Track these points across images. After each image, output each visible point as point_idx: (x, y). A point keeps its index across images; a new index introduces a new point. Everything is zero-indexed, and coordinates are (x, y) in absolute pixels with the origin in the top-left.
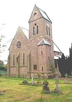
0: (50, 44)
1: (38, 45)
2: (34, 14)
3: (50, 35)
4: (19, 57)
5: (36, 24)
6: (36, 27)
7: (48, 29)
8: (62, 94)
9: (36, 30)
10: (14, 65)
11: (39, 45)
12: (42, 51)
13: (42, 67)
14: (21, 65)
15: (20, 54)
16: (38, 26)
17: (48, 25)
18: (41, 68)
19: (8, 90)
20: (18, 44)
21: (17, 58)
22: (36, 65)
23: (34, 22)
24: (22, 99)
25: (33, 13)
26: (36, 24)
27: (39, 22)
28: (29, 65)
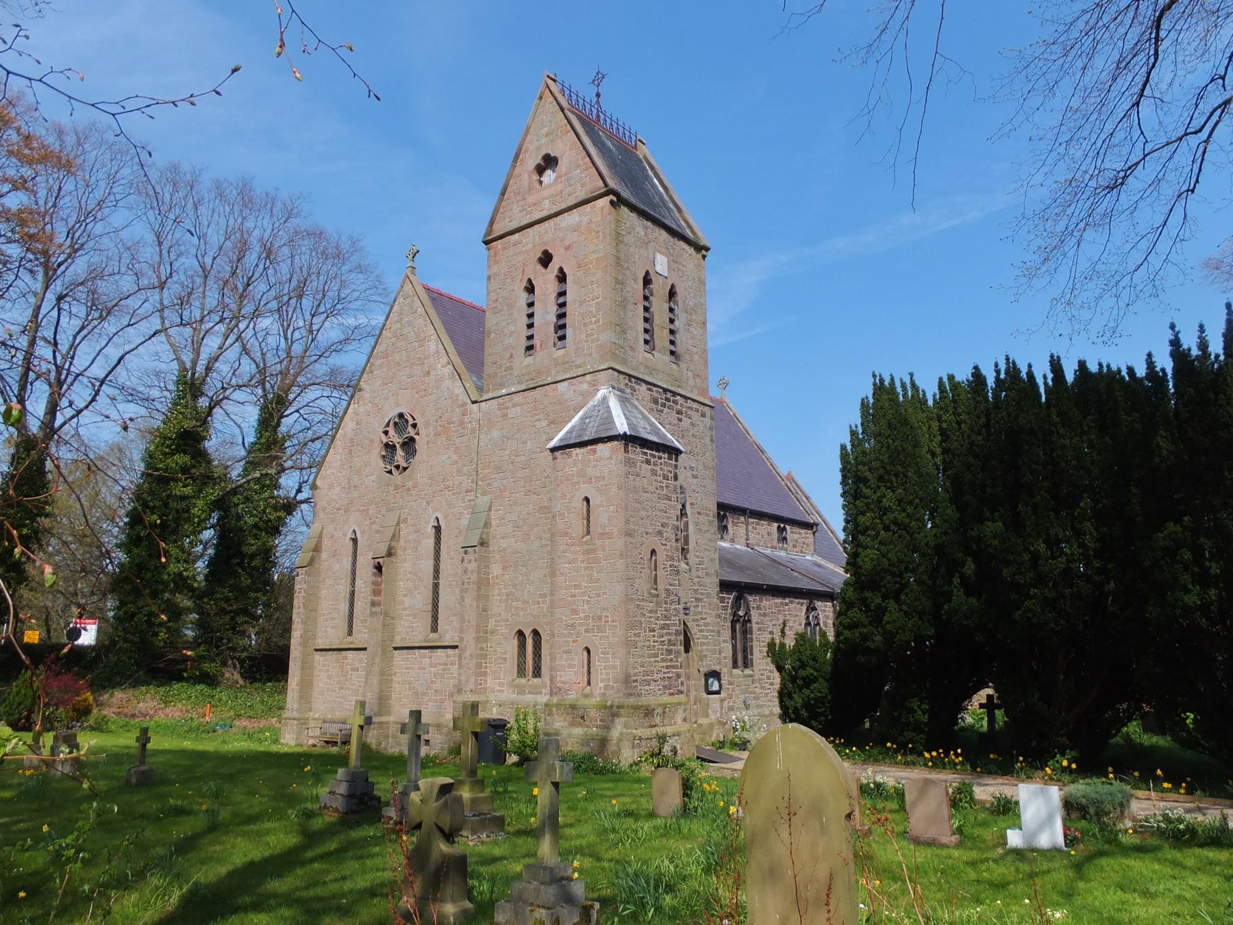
0: (711, 404)
1: (552, 444)
2: (540, 170)
4: (390, 554)
5: (546, 259)
6: (546, 282)
7: (659, 307)
9: (546, 315)
12: (587, 500)
14: (412, 627)
16: (562, 277)
17: (661, 265)
19: (119, 156)
22: (536, 633)
23: (532, 242)
24: (141, 618)
26: (546, 259)
27: (572, 238)
28: (470, 635)
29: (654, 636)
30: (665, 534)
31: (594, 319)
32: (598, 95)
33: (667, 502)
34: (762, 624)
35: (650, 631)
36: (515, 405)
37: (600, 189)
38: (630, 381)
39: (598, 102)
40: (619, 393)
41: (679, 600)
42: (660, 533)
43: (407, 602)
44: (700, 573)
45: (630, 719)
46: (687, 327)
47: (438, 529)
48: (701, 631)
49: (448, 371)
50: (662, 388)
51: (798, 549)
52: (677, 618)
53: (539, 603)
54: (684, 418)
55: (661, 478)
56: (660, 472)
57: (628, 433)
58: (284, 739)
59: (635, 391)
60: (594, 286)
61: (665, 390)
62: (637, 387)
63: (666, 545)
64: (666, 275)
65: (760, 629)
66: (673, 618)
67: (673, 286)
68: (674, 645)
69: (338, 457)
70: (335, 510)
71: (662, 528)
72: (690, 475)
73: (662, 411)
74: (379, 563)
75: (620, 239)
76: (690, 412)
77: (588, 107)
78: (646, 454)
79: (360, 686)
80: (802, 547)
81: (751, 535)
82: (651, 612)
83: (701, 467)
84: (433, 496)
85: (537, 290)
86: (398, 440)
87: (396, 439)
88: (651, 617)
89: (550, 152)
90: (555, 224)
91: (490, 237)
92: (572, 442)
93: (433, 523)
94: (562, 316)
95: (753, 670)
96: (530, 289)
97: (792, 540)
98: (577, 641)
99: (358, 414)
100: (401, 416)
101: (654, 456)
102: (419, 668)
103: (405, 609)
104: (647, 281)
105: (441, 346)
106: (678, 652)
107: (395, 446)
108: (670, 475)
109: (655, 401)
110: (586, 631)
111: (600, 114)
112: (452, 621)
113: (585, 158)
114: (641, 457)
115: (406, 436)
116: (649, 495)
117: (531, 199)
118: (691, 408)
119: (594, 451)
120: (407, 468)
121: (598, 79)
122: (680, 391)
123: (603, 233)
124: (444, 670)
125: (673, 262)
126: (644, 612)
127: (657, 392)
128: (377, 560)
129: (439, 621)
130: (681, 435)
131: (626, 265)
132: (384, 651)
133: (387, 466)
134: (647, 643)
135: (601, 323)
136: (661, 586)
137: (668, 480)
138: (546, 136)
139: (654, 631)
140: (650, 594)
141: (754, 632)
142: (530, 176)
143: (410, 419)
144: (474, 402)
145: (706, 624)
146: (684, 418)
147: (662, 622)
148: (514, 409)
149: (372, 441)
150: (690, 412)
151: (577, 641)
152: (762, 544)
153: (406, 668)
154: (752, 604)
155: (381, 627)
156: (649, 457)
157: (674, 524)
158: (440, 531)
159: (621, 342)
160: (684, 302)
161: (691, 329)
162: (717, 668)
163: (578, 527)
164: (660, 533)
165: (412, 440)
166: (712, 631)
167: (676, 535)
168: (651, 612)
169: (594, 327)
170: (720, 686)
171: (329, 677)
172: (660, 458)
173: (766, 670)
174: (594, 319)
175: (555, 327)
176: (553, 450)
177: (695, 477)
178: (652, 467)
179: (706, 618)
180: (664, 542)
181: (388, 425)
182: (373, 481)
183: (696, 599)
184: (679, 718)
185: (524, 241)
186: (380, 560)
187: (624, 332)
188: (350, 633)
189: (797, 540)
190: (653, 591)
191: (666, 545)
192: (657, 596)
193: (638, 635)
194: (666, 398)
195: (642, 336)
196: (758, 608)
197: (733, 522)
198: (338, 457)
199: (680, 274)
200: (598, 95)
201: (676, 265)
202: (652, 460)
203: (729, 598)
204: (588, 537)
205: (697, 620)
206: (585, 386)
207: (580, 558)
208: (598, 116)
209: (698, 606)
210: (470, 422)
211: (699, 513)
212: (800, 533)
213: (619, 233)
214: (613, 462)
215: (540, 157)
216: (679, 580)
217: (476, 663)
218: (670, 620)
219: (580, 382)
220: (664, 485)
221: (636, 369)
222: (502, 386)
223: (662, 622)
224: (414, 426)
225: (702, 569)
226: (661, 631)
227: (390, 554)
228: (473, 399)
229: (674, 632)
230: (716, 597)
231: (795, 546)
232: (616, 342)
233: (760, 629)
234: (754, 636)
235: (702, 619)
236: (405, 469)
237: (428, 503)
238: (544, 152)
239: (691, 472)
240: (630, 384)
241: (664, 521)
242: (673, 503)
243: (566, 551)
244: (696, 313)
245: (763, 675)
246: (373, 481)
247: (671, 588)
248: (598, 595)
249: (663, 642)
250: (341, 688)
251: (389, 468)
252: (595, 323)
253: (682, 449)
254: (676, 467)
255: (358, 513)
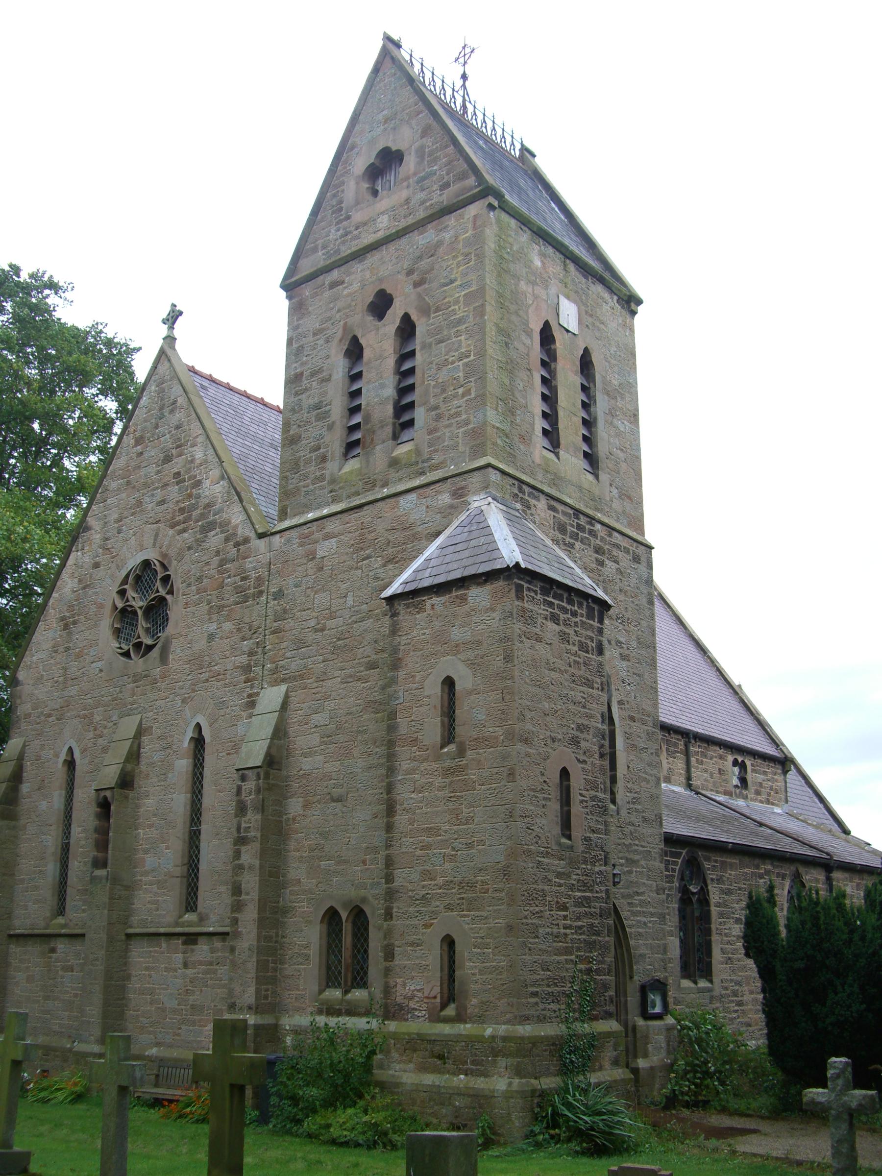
1: (395, 588)
3: (591, 458)
8: (26, 532)
10: (61, 910)
11: (412, 595)
12: (449, 683)
13: (449, 943)
15: (150, 749)
16: (407, 329)
18: (433, 957)
20: (138, 603)
21: (104, 806)
22: (359, 915)
25: (360, 163)
28: (250, 916)
29: (565, 918)
30: (583, 744)
31: (461, 391)
32: (464, 77)
33: (585, 689)
34: (726, 906)
35: (559, 909)
36: (327, 537)
37: (471, 189)
38: (521, 490)
39: (464, 86)
40: (504, 508)
41: (606, 857)
42: (575, 742)
43: (150, 861)
44: (633, 819)
45: (526, 1060)
46: (609, 418)
47: (199, 742)
48: (635, 914)
49: (220, 489)
50: (572, 508)
51: (763, 797)
52: (603, 888)
53: (364, 862)
54: (607, 562)
55: (576, 648)
56: (574, 638)
57: (523, 566)
58: (740, 928)
59: (529, 508)
60: (462, 338)
61: (578, 512)
62: (533, 502)
63: (585, 762)
64: (576, 333)
65: (721, 915)
66: (597, 888)
67: (586, 352)
68: (598, 934)
69: (50, 634)
70: (43, 718)
71: (578, 734)
72: (617, 655)
73: (572, 546)
74: (105, 798)
75: (504, 266)
76: (615, 552)
77: (449, 92)
78: (551, 604)
79: (76, 995)
80: (769, 795)
81: (694, 773)
82: (559, 875)
83: (634, 644)
84: (194, 691)
85: (367, 354)
86: (141, 604)
87: (138, 603)
88: (560, 885)
89: (390, 144)
90: (397, 250)
91: (293, 279)
92: (426, 583)
93: (190, 733)
94: (405, 390)
95: (711, 981)
96: (355, 351)
97: (755, 783)
98: (432, 924)
99: (82, 567)
100: (146, 564)
101: (564, 610)
102: (167, 969)
103: (146, 873)
104: (547, 336)
105: (211, 451)
106: (605, 947)
107: (135, 613)
108: (590, 643)
109: (562, 529)
110: (449, 908)
111: (468, 104)
112: (220, 893)
113: (446, 147)
114: (541, 610)
115: (153, 596)
116: (555, 675)
117: (358, 217)
118: (618, 546)
119: (463, 599)
120: (153, 646)
121: (465, 54)
122: (599, 516)
123: (476, 255)
124: (206, 972)
125: (586, 315)
126: (551, 876)
127: (564, 513)
128: (102, 794)
129: (200, 893)
130: (605, 584)
131: (513, 308)
132: (111, 939)
133: (123, 646)
134: (555, 930)
135: (473, 395)
136: (577, 833)
137: (587, 652)
138: (385, 122)
139: (565, 908)
140: (560, 844)
141: (713, 920)
142: (357, 183)
143: (158, 568)
144: (261, 536)
145: (642, 903)
146: (607, 562)
147: (579, 894)
148: (327, 543)
149: (101, 606)
150: (615, 552)
151: (432, 924)
152: (710, 786)
153: (147, 969)
154: (711, 875)
155: (107, 900)
156: (556, 611)
157: (597, 728)
158: (203, 747)
159: (506, 427)
160: (604, 377)
161: (615, 421)
162: (660, 975)
163: (433, 730)
164: (575, 742)
165: (162, 600)
166: (652, 915)
167: (602, 746)
168: (559, 875)
169: (461, 402)
170: (665, 1005)
171: (30, 979)
172: (574, 614)
173: (732, 980)
174: (461, 391)
175: (395, 408)
176: (390, 599)
177: (624, 657)
178: (562, 628)
179: (642, 893)
180: (582, 758)
181: (125, 581)
182: (101, 671)
183: (627, 859)
184: (607, 1059)
185: (347, 279)
186: (108, 794)
187: (512, 412)
188: (61, 910)
189: (761, 784)
190: (564, 841)
191: (585, 762)
192: (571, 848)
193: (539, 915)
194: (578, 525)
195: (540, 424)
196: (719, 880)
197: (667, 750)
198: (50, 634)
199: (597, 334)
200: (464, 77)
201: (590, 320)
202: (562, 616)
203: (675, 863)
204: (452, 748)
205: (629, 896)
206: (445, 499)
207: (438, 781)
208: (464, 106)
209: (630, 872)
210: (255, 568)
211: (632, 719)
212: (765, 773)
213: (502, 258)
214: (497, 615)
215: (374, 153)
216: (606, 824)
217: (257, 961)
218: (591, 891)
219: (438, 492)
220: (581, 660)
221: (532, 474)
222: (308, 508)
223: (579, 894)
224: (166, 579)
225: (637, 810)
226: (578, 910)
227: (126, 782)
228: (260, 531)
229: (598, 911)
230: (658, 860)
231: (758, 793)
232: (498, 425)
233: (721, 915)
234: (713, 926)
235: (638, 894)
236: (150, 648)
237: (184, 701)
238: (380, 146)
239: (619, 651)
240: (521, 495)
241: (580, 721)
242: (595, 692)
243: (413, 771)
244: (622, 398)
245: (726, 988)
246: (101, 671)
247: (593, 836)
248: (469, 845)
249: (580, 927)
250: (47, 998)
251: (126, 648)
252: (463, 395)
253: (610, 602)
254: (600, 631)
255: (76, 721)
